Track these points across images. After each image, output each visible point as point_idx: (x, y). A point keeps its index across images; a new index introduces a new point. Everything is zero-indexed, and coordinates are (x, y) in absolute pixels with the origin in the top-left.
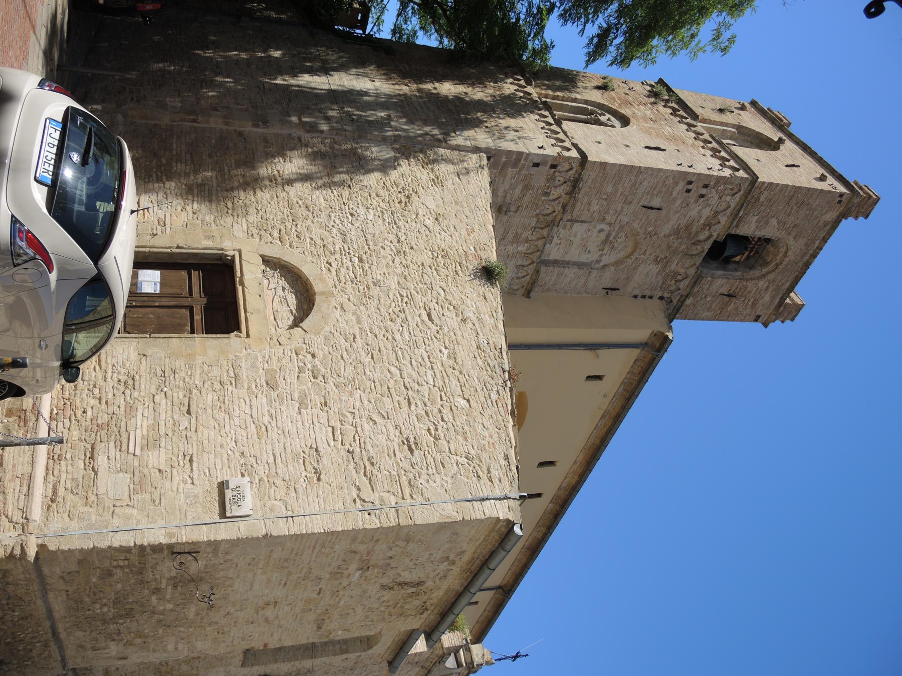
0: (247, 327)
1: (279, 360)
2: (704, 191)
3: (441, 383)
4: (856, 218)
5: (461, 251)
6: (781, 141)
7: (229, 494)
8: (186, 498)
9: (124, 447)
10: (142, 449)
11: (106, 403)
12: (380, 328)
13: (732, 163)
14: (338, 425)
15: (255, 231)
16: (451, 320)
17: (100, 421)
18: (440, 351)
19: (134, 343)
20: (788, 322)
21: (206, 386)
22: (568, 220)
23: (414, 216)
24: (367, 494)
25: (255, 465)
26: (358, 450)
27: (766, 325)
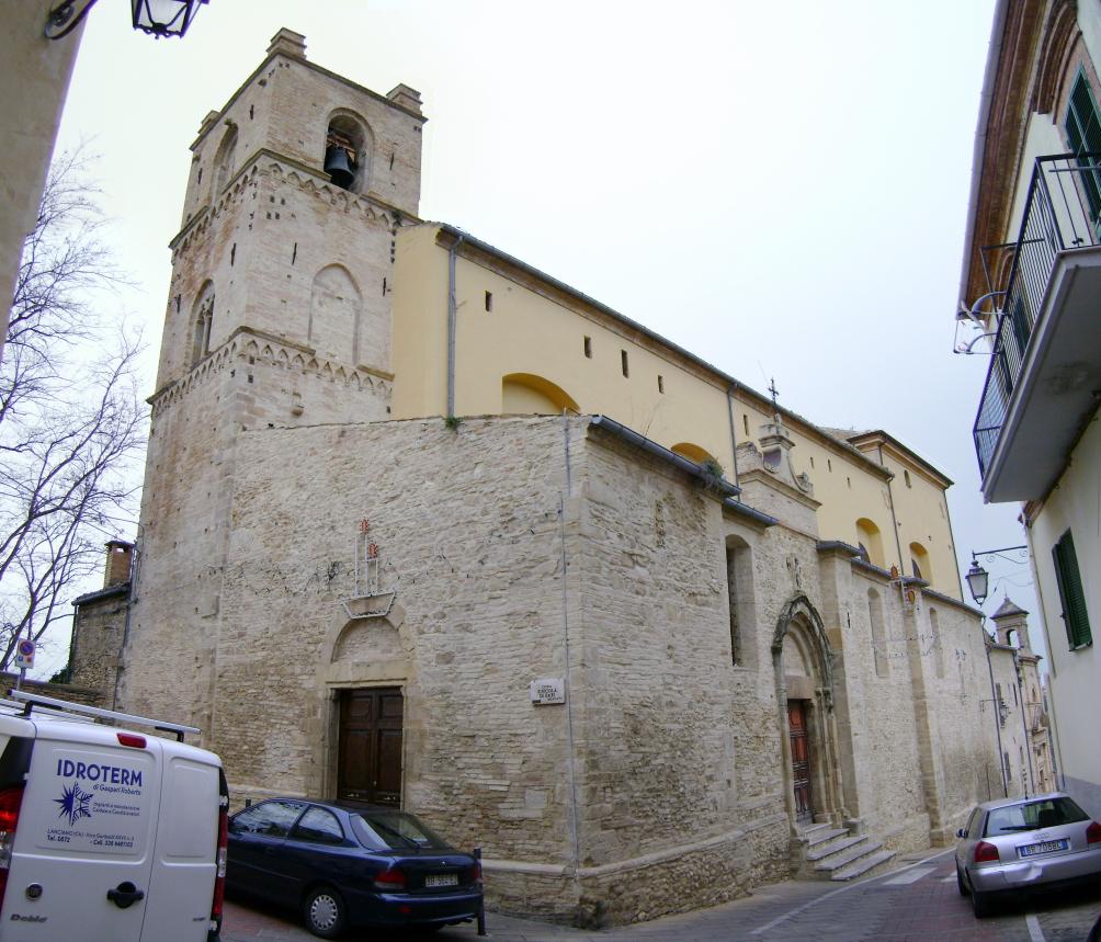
0: (398, 680)
1: (428, 651)
2: (278, 200)
3: (459, 493)
4: (304, 47)
5: (332, 463)
6: (228, 123)
7: (544, 700)
8: (547, 739)
9: (503, 795)
10: (505, 779)
11: (465, 810)
12: (399, 549)
13: (249, 173)
14: (486, 594)
15: (309, 667)
16: (399, 476)
17: (480, 816)
18: (426, 489)
19: (409, 784)
20: (421, 98)
21: (449, 721)
22: (309, 338)
23: (298, 511)
24: (551, 565)
25: (521, 675)
26: (510, 574)
27: (424, 120)
